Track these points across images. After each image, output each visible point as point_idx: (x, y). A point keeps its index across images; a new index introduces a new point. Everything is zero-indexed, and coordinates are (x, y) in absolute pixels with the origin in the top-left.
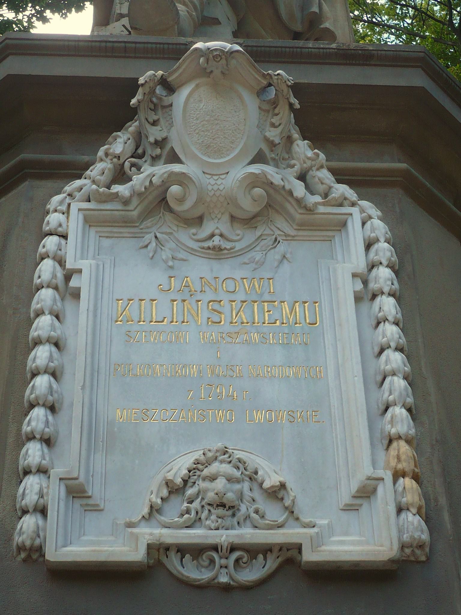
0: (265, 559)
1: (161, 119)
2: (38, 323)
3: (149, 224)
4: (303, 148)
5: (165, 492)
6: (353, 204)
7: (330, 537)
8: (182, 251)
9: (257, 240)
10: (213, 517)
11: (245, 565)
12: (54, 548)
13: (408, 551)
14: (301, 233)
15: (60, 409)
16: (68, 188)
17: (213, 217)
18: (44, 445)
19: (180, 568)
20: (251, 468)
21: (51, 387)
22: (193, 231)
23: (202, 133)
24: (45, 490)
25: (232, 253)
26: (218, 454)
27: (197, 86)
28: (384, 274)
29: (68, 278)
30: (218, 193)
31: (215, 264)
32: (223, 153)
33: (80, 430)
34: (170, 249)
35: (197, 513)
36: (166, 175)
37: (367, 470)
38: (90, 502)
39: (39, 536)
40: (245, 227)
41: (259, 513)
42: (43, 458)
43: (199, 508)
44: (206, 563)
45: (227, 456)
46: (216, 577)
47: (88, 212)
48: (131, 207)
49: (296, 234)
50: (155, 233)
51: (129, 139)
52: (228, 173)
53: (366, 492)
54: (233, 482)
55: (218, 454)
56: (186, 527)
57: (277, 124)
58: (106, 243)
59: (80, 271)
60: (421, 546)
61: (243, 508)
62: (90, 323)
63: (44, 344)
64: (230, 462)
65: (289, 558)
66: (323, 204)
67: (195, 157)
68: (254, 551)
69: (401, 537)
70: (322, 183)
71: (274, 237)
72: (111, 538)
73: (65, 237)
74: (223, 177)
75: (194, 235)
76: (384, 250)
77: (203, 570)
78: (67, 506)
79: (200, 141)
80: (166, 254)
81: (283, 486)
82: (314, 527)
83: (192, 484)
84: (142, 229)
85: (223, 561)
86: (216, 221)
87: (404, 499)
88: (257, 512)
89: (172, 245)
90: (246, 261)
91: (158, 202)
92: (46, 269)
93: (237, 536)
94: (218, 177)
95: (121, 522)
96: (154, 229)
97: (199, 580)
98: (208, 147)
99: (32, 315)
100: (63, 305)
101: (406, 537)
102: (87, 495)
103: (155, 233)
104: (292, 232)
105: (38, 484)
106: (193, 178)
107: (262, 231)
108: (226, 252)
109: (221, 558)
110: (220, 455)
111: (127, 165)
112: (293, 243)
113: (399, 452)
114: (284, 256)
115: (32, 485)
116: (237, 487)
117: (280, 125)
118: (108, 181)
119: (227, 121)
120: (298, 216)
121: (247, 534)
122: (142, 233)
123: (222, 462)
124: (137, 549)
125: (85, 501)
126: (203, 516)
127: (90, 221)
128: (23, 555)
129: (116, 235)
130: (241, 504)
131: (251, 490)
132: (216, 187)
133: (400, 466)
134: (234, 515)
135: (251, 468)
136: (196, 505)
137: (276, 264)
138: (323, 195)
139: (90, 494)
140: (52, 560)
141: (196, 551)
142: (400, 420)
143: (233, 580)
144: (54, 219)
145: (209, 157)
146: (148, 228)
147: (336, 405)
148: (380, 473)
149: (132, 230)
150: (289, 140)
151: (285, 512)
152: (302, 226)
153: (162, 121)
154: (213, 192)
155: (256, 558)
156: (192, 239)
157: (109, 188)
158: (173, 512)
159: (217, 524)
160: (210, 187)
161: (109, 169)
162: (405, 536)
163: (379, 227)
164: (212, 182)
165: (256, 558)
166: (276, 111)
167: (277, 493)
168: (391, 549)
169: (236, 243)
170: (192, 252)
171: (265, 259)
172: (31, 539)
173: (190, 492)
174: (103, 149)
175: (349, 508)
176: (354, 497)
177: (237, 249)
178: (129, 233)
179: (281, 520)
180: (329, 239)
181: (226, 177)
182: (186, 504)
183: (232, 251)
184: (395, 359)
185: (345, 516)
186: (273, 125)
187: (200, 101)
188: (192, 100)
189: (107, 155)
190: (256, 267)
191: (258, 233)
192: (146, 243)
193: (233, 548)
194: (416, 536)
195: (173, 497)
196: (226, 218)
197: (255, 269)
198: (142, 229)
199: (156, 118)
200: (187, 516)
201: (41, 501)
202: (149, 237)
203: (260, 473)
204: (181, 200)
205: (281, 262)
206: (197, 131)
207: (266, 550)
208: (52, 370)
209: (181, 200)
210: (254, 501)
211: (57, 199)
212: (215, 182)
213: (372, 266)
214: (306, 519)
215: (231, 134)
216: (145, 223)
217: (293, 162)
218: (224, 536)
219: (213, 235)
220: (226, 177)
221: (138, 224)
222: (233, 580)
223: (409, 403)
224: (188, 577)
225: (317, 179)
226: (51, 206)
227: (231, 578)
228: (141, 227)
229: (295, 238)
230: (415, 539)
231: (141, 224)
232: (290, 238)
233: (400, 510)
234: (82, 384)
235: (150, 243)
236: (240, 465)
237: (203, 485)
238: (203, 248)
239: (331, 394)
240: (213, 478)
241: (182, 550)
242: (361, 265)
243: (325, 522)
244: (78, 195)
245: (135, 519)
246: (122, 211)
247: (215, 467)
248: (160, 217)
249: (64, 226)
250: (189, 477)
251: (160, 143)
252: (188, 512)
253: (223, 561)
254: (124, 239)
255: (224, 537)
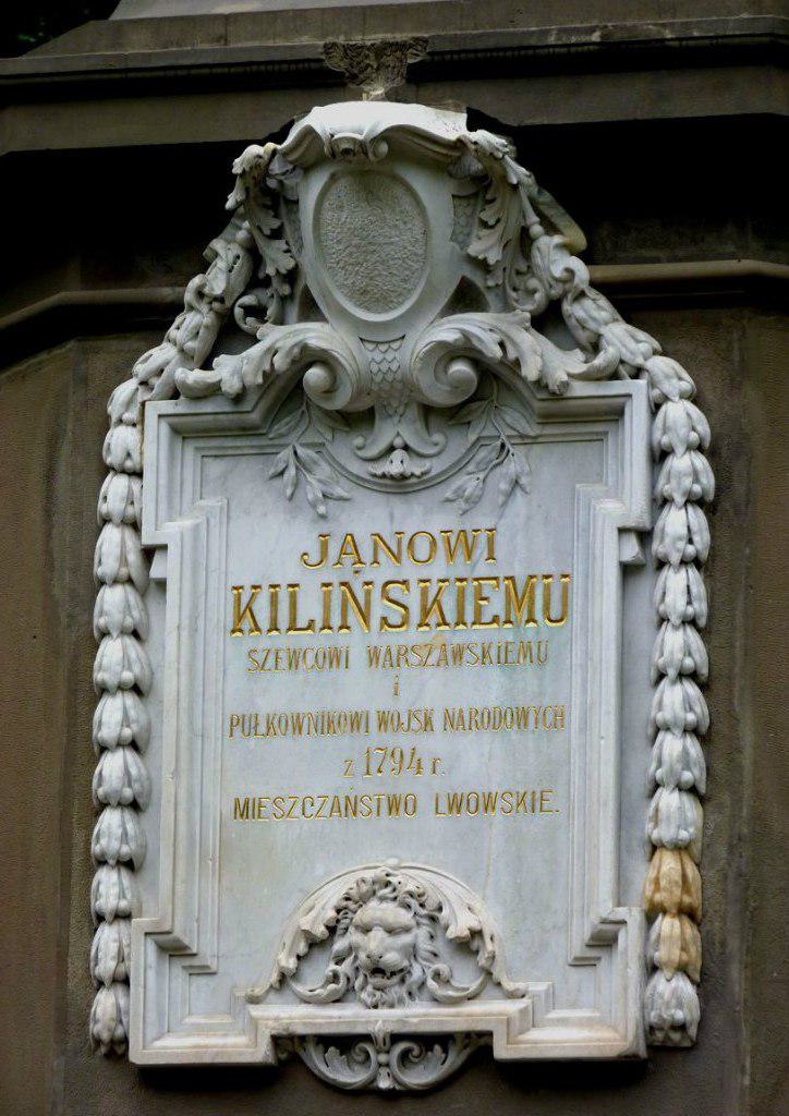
0: (446, 1051)
1: (286, 224)
2: (101, 660)
3: (283, 430)
4: (558, 258)
5: (302, 948)
6: (637, 373)
7: (548, 1012)
8: (343, 480)
9: (469, 450)
10: (369, 988)
11: (417, 1060)
12: (141, 1044)
13: (659, 1035)
14: (549, 430)
15: (147, 805)
16: (141, 368)
17: (390, 412)
18: (124, 872)
19: (323, 1068)
20: (431, 904)
21: (127, 772)
22: (359, 441)
23: (350, 268)
24: (126, 951)
25: (428, 481)
26: (376, 887)
27: (333, 178)
28: (681, 527)
29: (149, 553)
30: (390, 377)
31: (397, 503)
32: (392, 302)
33: (172, 850)
34: (320, 481)
35: (348, 979)
36: (296, 350)
37: (605, 907)
38: (196, 962)
39: (121, 1022)
40: (450, 423)
41: (442, 977)
42: (122, 895)
43: (350, 973)
44: (361, 1058)
45: (389, 889)
46: (374, 1080)
47: (176, 420)
48: (247, 407)
49: (538, 432)
50: (294, 447)
51: (238, 257)
52: (403, 337)
53: (604, 941)
54: (396, 934)
55: (376, 887)
56: (334, 1002)
57: (491, 222)
58: (215, 468)
59: (164, 548)
60: (681, 1027)
61: (417, 972)
62: (185, 650)
63: (114, 694)
64: (396, 898)
65: (478, 1044)
66: (585, 377)
67: (343, 314)
68: (428, 1042)
69: (647, 1017)
70: (584, 328)
71: (499, 443)
72: (227, 1020)
73: (138, 474)
74: (395, 345)
75: (360, 449)
76: (689, 470)
77: (356, 1068)
78: (159, 973)
79: (350, 282)
80: (313, 489)
81: (476, 934)
82: (523, 996)
83: (342, 931)
84: (271, 439)
85: (383, 1058)
86: (396, 419)
87: (657, 954)
88: (437, 975)
89: (324, 470)
90: (449, 494)
91: (286, 394)
92: (111, 546)
93: (401, 1021)
94: (386, 346)
95: (241, 994)
96: (292, 439)
97: (350, 1084)
98: (364, 292)
99: (96, 634)
100: (145, 609)
101: (653, 1017)
102: (189, 952)
103: (294, 447)
104: (533, 430)
105: (115, 941)
106: (341, 359)
107: (478, 431)
108: (413, 480)
109: (378, 1052)
110: (381, 888)
111: (238, 311)
112: (537, 449)
113: (659, 872)
114: (517, 482)
115: (107, 938)
116: (406, 939)
117: (498, 221)
118: (208, 348)
119: (392, 243)
120: (537, 405)
121: (419, 1015)
122: (273, 446)
123: (383, 899)
124: (256, 1044)
125: (188, 962)
126: (358, 984)
127: (182, 432)
128: (103, 1050)
129: (230, 452)
130: (414, 964)
131: (432, 937)
132: (384, 367)
133: (658, 897)
134: (403, 981)
135: (431, 904)
136: (345, 968)
137: (501, 499)
138: (589, 347)
139: (194, 951)
140: (138, 1063)
141: (345, 1043)
142: (676, 814)
143: (400, 1084)
144: (119, 440)
145: (368, 309)
146: (282, 436)
147: (577, 780)
148: (621, 913)
149: (255, 442)
150: (525, 241)
151: (476, 979)
152: (547, 419)
153: (288, 230)
154: (380, 376)
155: (432, 1050)
156: (355, 454)
157: (207, 365)
158: (315, 978)
159: (374, 999)
160: (375, 368)
161: (207, 327)
162: (653, 1014)
163: (683, 419)
164: (378, 357)
165: (432, 1050)
166: (488, 197)
167: (468, 945)
168: (625, 1038)
169: (434, 460)
170: (358, 481)
171: (483, 489)
172: (109, 1030)
173: (340, 944)
174: (196, 281)
175: (580, 963)
176: (589, 946)
177: (433, 473)
178: (253, 447)
179: (473, 987)
180: (599, 437)
181: (400, 346)
182: (333, 966)
183: (425, 478)
184: (678, 700)
185: (576, 975)
186: (484, 225)
187: (341, 208)
188: (326, 205)
189: (200, 294)
190: (467, 507)
191: (472, 437)
192: (280, 469)
193: (396, 1038)
194: (665, 1016)
195: (316, 951)
196: (413, 412)
197: (465, 512)
198: (271, 439)
199: (275, 224)
200: (333, 986)
201: (122, 969)
202: (286, 454)
203: (445, 912)
204: (330, 391)
205: (509, 495)
206: (341, 264)
207: (444, 1040)
208: (130, 739)
209: (330, 391)
210: (435, 955)
211: (124, 391)
212: (382, 356)
213: (660, 503)
214: (509, 985)
215: (400, 265)
216: (276, 427)
217: (533, 283)
218: (380, 1022)
219: (392, 449)
220: (400, 346)
221: (265, 431)
222: (400, 1084)
223: (687, 782)
224: (335, 1080)
225: (573, 320)
226: (114, 409)
227: (395, 1080)
228: (271, 436)
229: (540, 440)
230: (664, 1020)
231: (270, 427)
232: (529, 441)
233: (652, 968)
234: (172, 768)
235: (286, 467)
236: (413, 902)
237: (354, 937)
238: (375, 475)
239: (572, 761)
240: (366, 930)
241: (325, 1041)
242: (635, 509)
243: (542, 987)
244: (157, 382)
245: (258, 991)
246: (233, 413)
247: (373, 910)
248: (303, 412)
249: (136, 455)
250: (338, 921)
251: (292, 277)
252: (335, 978)
253: (383, 1058)
254: (245, 458)
255: (380, 1021)
